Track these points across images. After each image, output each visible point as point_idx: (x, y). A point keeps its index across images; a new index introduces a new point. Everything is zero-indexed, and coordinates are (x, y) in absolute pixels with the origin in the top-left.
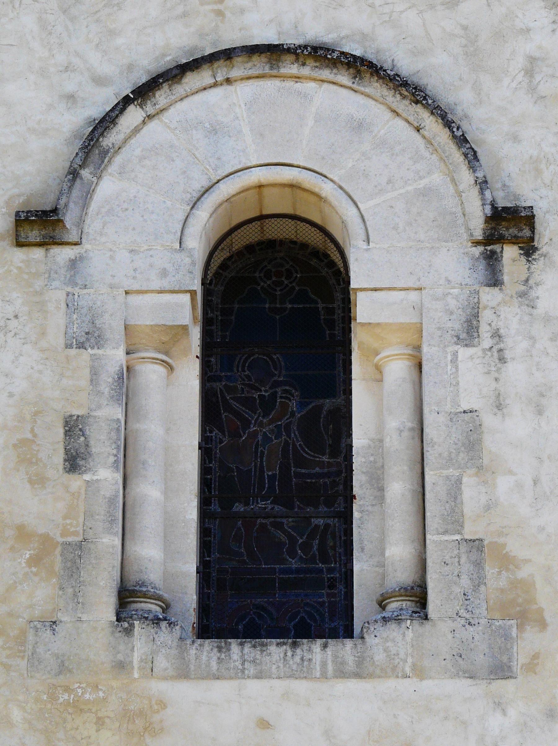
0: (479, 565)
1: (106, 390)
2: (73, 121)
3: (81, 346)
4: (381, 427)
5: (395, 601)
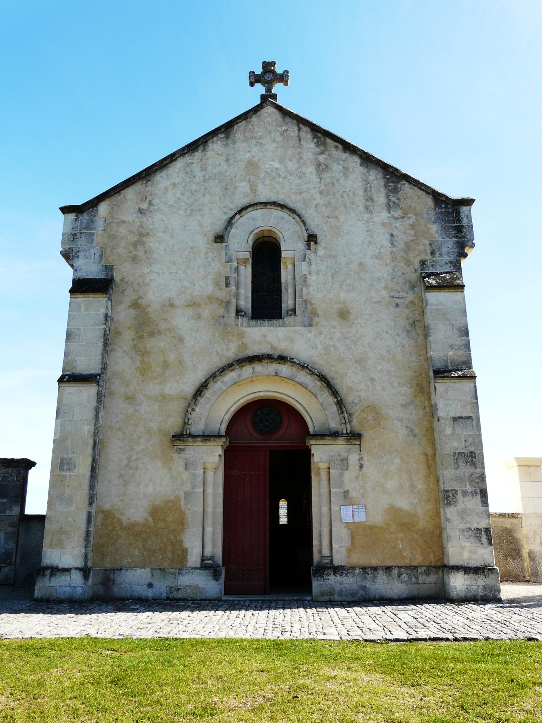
0: (306, 304)
1: (233, 271)
2: (226, 218)
3: (228, 262)
4: (287, 278)
5: (525, 606)
